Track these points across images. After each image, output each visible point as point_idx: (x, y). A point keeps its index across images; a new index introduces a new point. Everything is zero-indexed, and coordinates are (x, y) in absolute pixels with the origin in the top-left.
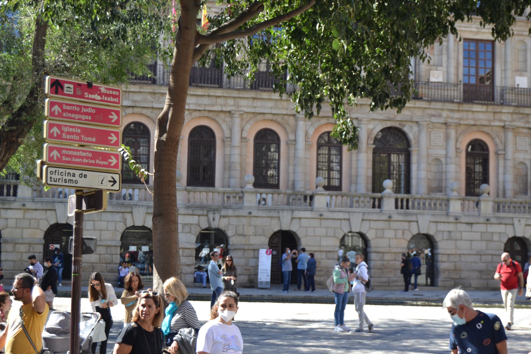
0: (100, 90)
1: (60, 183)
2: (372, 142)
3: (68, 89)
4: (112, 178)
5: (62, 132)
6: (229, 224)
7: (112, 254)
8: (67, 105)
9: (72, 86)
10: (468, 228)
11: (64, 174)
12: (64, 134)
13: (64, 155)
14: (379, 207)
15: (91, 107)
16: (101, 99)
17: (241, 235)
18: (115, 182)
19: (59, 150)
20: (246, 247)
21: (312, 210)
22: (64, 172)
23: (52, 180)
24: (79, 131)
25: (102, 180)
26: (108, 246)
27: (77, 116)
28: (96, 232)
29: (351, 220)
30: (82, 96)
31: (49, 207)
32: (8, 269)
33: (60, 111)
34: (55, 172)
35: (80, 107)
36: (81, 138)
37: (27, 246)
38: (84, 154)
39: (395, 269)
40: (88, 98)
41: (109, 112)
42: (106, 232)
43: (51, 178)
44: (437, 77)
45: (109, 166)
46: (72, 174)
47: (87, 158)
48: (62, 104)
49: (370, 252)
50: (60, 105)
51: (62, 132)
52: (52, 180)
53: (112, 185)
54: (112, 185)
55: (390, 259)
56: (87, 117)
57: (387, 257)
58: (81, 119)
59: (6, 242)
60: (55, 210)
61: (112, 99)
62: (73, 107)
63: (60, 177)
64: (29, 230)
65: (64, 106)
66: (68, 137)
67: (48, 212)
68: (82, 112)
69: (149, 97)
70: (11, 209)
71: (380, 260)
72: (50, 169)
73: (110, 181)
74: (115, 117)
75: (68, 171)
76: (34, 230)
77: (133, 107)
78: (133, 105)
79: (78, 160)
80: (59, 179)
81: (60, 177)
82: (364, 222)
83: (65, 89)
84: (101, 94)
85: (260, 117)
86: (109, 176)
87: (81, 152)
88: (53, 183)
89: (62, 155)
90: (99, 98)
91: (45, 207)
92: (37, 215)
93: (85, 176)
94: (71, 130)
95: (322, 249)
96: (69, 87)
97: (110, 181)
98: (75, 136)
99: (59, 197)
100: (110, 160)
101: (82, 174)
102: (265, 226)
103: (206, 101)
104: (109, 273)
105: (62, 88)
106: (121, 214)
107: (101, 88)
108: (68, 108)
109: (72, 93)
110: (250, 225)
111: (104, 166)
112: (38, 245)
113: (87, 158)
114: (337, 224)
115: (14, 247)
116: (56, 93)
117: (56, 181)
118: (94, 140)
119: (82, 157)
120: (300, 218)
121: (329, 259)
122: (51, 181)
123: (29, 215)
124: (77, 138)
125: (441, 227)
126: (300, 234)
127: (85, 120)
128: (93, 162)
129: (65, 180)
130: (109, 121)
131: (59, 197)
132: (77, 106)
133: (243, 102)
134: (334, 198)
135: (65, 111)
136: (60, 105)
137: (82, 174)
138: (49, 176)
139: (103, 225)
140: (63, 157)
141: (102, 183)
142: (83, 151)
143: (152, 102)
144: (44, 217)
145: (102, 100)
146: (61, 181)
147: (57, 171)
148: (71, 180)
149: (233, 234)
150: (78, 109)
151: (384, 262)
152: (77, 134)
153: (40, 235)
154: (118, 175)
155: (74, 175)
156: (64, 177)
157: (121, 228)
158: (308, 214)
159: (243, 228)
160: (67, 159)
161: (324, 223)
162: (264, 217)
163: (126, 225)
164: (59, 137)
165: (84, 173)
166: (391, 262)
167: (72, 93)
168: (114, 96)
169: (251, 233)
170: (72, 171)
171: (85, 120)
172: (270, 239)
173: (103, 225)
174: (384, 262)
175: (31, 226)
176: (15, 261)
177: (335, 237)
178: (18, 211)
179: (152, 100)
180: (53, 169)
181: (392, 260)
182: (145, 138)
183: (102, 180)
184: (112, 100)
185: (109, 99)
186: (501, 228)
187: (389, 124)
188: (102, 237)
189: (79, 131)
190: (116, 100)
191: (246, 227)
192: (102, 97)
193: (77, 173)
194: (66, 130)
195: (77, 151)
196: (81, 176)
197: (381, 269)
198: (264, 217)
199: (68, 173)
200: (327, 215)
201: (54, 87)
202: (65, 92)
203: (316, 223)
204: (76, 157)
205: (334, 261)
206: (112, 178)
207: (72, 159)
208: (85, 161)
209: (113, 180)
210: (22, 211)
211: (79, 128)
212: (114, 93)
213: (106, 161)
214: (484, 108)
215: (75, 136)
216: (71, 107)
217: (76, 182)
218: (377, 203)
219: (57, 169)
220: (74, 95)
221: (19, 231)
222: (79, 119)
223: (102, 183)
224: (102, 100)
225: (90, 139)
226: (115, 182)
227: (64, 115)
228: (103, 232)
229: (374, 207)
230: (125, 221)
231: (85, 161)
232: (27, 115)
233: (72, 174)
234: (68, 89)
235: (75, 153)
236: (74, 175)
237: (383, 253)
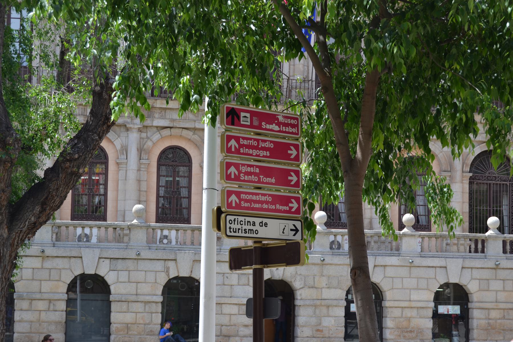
0: (278, 119)
1: (240, 234)
2: (468, 169)
3: (245, 118)
4: (294, 225)
5: (240, 172)
6: (296, 273)
7: (152, 313)
8: (244, 138)
9: (248, 115)
11: (244, 223)
12: (241, 175)
13: (242, 200)
14: (483, 251)
15: (268, 141)
16: (279, 129)
17: (312, 287)
18: (297, 230)
19: (238, 194)
20: (318, 303)
21: (399, 255)
22: (244, 221)
23: (232, 230)
24: (258, 170)
25: (284, 229)
26: (146, 303)
27: (255, 152)
28: (132, 284)
29: (448, 268)
30: (260, 127)
31: (74, 254)
32: (24, 331)
33: (237, 146)
34: (234, 221)
35: (258, 140)
36: (259, 178)
37: (46, 303)
38: (263, 198)
39: (503, 330)
40: (266, 129)
41: (287, 146)
42: (144, 284)
43: (230, 228)
45: (289, 212)
46: (252, 223)
47: (267, 202)
48: (239, 137)
49: (297, 299)
50: (237, 139)
51: (240, 172)
52: (232, 230)
53: (294, 235)
54: (294, 235)
55: (498, 317)
56: (265, 153)
57: (494, 314)
58: (259, 156)
59: (22, 298)
60: (81, 257)
61: (291, 130)
62: (251, 142)
63: (239, 226)
64: (49, 282)
65: (241, 140)
66: (246, 178)
67: (73, 260)
68: (260, 147)
70: (26, 256)
71: (486, 319)
72: (229, 218)
73: (292, 230)
74: (294, 152)
75: (248, 219)
76: (56, 282)
77: (171, 128)
78: (171, 125)
79: (257, 206)
80: (239, 229)
81: (239, 226)
82: (464, 270)
83: (242, 119)
84: (279, 124)
86: (290, 224)
87: (260, 196)
88: (233, 234)
89: (240, 200)
90: (277, 128)
91: (68, 254)
92: (60, 263)
93: (266, 225)
94: (249, 169)
95: (414, 304)
96: (245, 117)
97: (292, 230)
98: (253, 177)
100: (290, 205)
101: (262, 222)
102: (341, 276)
104: (148, 336)
105: (239, 118)
106: (163, 262)
107: (278, 117)
108: (245, 142)
109: (249, 124)
110: (322, 275)
111: (285, 212)
112: (60, 302)
113: (267, 202)
114: (431, 273)
115: (31, 303)
116: (233, 124)
117: (236, 232)
118: (273, 180)
119: (262, 202)
120: (385, 266)
121: (421, 317)
122: (231, 232)
123: (48, 264)
124: (256, 179)
127: (263, 156)
128: (274, 207)
129: (245, 230)
130: (288, 157)
132: (255, 140)
134: (426, 239)
135: (241, 146)
136: (237, 139)
137: (262, 222)
138: (228, 225)
139: (139, 276)
140: (242, 202)
141: (283, 233)
142: (263, 195)
143: (195, 121)
144: (67, 266)
145: (279, 131)
146: (240, 231)
147: (236, 220)
148: (251, 230)
149: (301, 286)
150: (255, 143)
151: (490, 321)
152: (255, 174)
153: (64, 288)
154: (300, 222)
155: (254, 224)
156: (244, 227)
157: (163, 280)
158: (394, 260)
159: (314, 278)
160: (247, 205)
161: (415, 272)
162: (340, 265)
163: (168, 275)
164: (237, 178)
165: (265, 220)
166: (499, 321)
167: (249, 124)
168: (293, 126)
169: (324, 285)
170: (251, 219)
171: (263, 156)
172: (103, 278)
173: (139, 276)
174: (490, 321)
175: (51, 278)
176: (31, 322)
177: (427, 289)
178: (34, 258)
179: (194, 118)
180: (232, 218)
181: (499, 319)
182: (186, 166)
183: (284, 229)
184: (290, 131)
185: (287, 130)
188: (138, 291)
189: (258, 170)
190: (294, 130)
191: (317, 278)
192: (280, 127)
193: (258, 221)
194: (244, 169)
195: (253, 194)
196: (261, 224)
197: (486, 330)
198: (340, 265)
199: (248, 222)
200: (418, 261)
201: (230, 117)
202: (242, 123)
203: (404, 272)
204: (256, 202)
205: (427, 320)
206: (294, 225)
207: (251, 205)
208: (265, 206)
209: (294, 228)
210: (41, 259)
211: (257, 166)
212: (293, 122)
213: (287, 205)
215: (253, 177)
216: (248, 141)
217: (257, 232)
218: (480, 246)
219: (236, 217)
220: (251, 126)
221: (36, 283)
222: (257, 156)
223: (283, 233)
224: (279, 131)
225: (269, 180)
226: (297, 230)
227: (242, 150)
228: (139, 285)
229: (476, 251)
230: (167, 272)
231: (265, 206)
233: (252, 223)
234: (245, 119)
235: (254, 198)
236: (254, 224)
237: (489, 309)
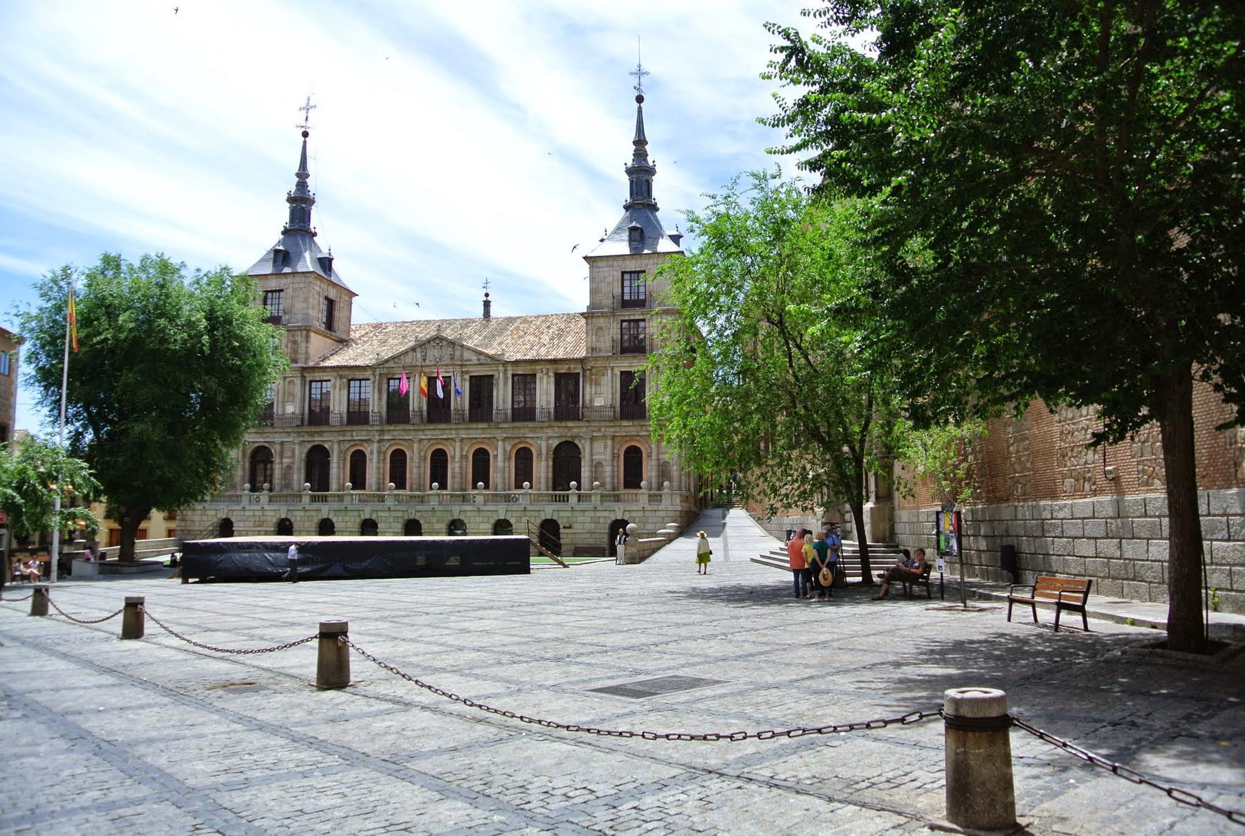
10: (582, 514)
44: (599, 402)
69: (403, 433)
85: (474, 441)
99: (431, 488)
103: (438, 432)
125: (562, 514)
126: (466, 521)
131: (431, 488)
133: (462, 432)
186: (606, 514)
187: (564, 440)
203: (475, 514)
214: (631, 424)
232: (1197, 72)
